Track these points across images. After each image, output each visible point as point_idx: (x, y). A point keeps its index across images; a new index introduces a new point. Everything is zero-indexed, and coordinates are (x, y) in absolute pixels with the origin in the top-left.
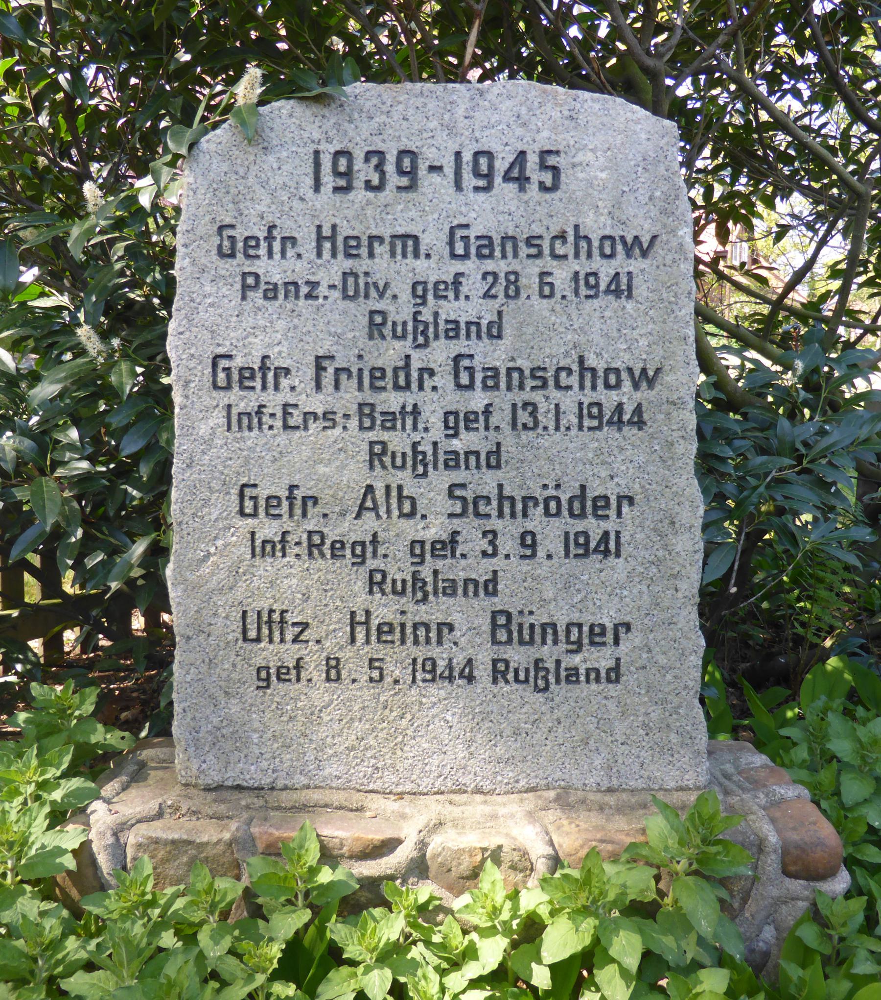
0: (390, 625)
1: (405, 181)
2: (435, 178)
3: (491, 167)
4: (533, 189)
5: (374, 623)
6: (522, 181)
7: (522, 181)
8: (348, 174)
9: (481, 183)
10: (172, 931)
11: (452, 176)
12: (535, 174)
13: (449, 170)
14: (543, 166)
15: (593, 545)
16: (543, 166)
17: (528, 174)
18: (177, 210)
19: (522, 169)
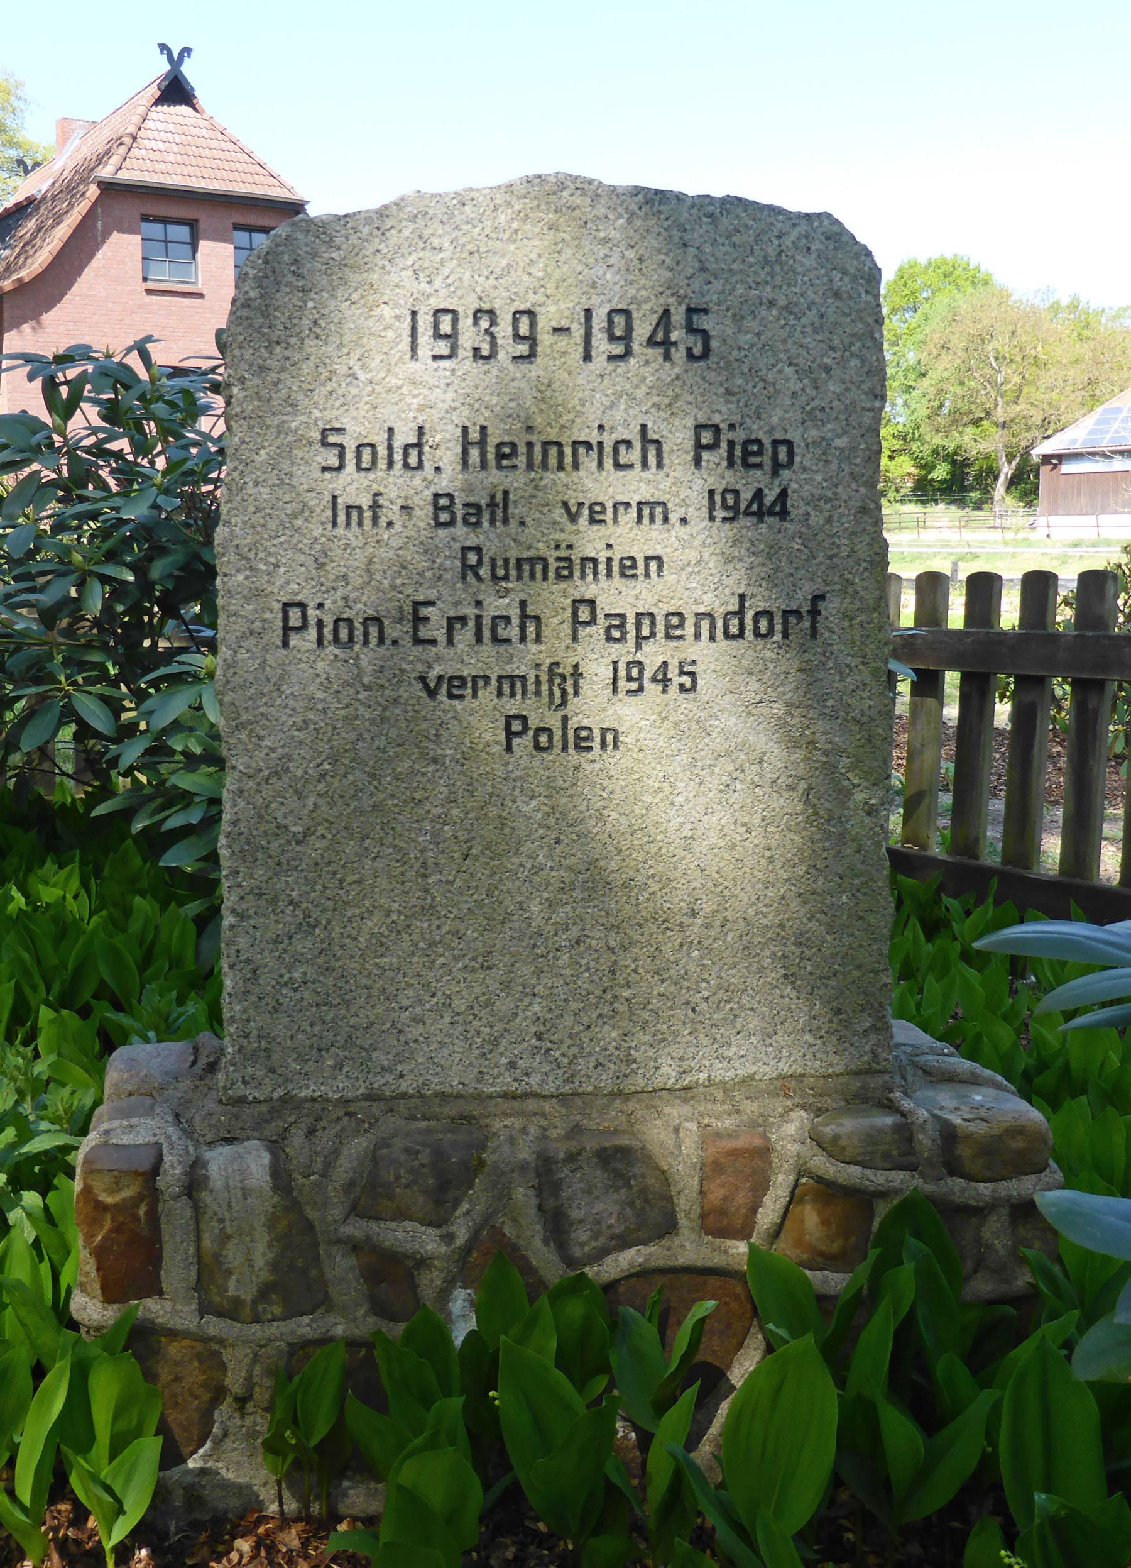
0: (513, 445)
1: (523, 348)
2: (563, 342)
3: (629, 328)
4: (673, 689)
5: (492, 441)
6: (665, 681)
7: (665, 681)
8: (452, 337)
9: (618, 349)
10: (692, 1455)
11: (598, 611)
12: (676, 680)
13: (578, 332)
14: (682, 673)
15: (743, 506)
16: (682, 673)
17: (669, 676)
18: (713, 1528)
19: (665, 674)
